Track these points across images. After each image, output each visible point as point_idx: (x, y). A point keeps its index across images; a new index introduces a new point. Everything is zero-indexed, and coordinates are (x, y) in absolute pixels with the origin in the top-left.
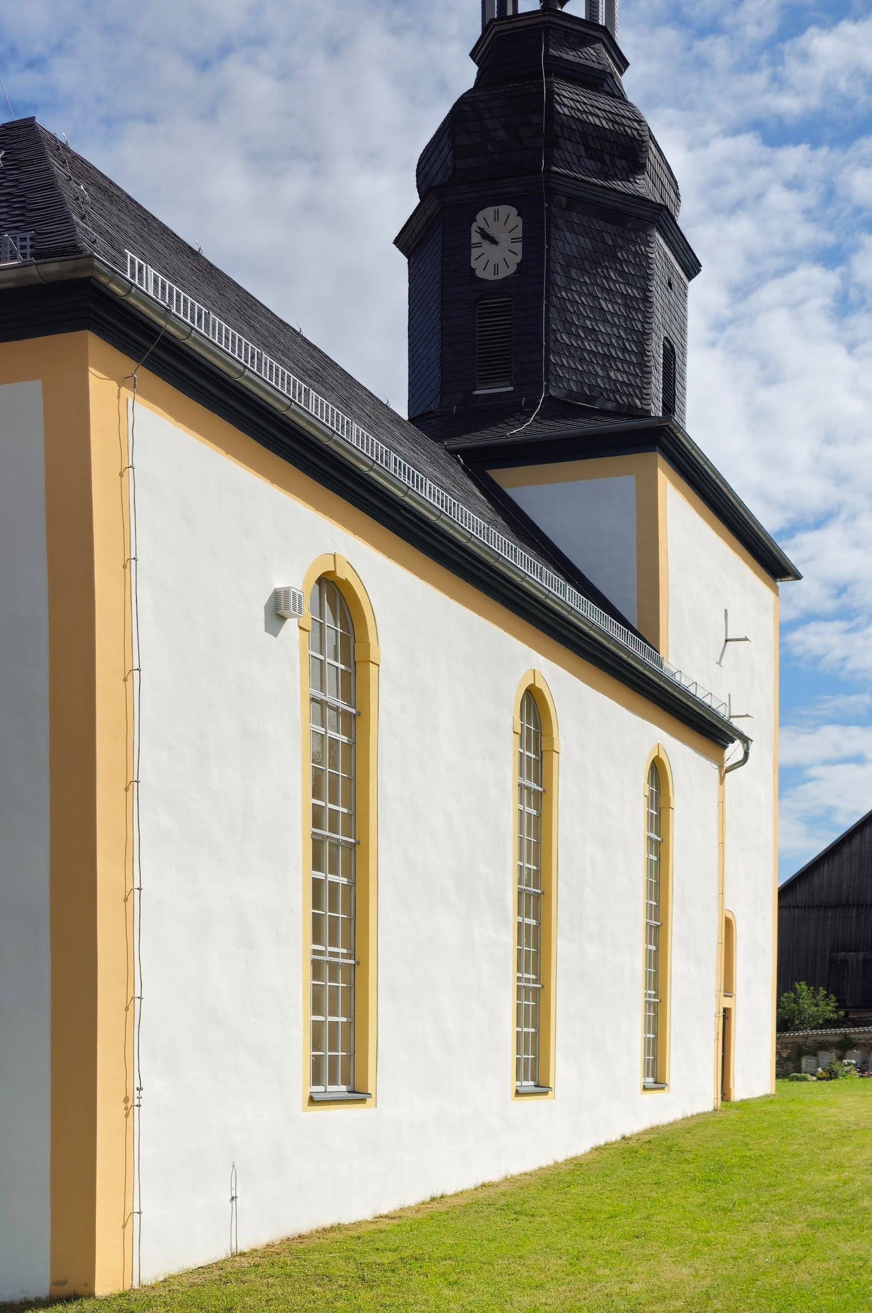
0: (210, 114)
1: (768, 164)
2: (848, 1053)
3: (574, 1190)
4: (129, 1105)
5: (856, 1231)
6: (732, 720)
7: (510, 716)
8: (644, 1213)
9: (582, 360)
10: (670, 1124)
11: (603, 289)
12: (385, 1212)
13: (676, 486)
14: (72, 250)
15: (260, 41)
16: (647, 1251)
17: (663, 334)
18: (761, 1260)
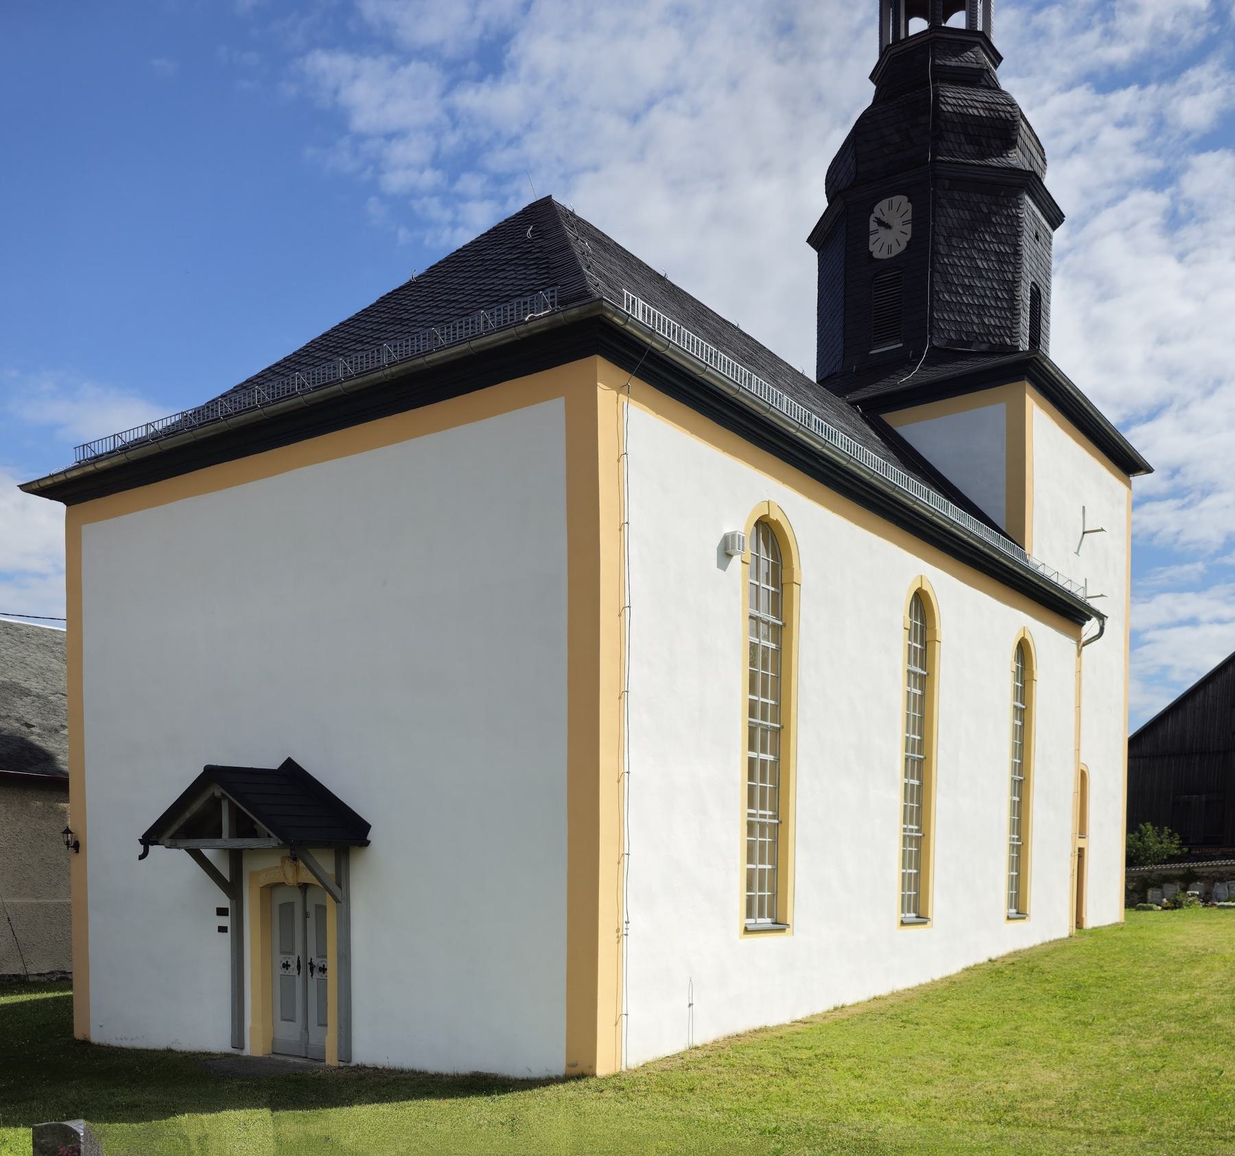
0: (640, 156)
1: (1100, 109)
2: (1191, 886)
3: (950, 1003)
4: (620, 934)
5: (1210, 1045)
6: (1089, 601)
7: (900, 615)
8: (1013, 1024)
9: (960, 312)
10: (1031, 949)
11: (979, 250)
12: (799, 1018)
13: (1042, 407)
14: (584, 294)
15: (676, 91)
16: (1019, 1057)
17: (1030, 279)
18: (1122, 1068)
